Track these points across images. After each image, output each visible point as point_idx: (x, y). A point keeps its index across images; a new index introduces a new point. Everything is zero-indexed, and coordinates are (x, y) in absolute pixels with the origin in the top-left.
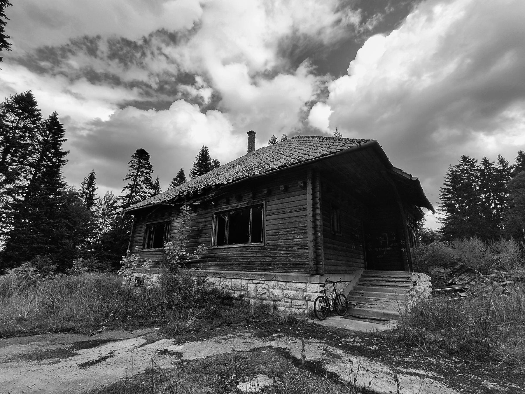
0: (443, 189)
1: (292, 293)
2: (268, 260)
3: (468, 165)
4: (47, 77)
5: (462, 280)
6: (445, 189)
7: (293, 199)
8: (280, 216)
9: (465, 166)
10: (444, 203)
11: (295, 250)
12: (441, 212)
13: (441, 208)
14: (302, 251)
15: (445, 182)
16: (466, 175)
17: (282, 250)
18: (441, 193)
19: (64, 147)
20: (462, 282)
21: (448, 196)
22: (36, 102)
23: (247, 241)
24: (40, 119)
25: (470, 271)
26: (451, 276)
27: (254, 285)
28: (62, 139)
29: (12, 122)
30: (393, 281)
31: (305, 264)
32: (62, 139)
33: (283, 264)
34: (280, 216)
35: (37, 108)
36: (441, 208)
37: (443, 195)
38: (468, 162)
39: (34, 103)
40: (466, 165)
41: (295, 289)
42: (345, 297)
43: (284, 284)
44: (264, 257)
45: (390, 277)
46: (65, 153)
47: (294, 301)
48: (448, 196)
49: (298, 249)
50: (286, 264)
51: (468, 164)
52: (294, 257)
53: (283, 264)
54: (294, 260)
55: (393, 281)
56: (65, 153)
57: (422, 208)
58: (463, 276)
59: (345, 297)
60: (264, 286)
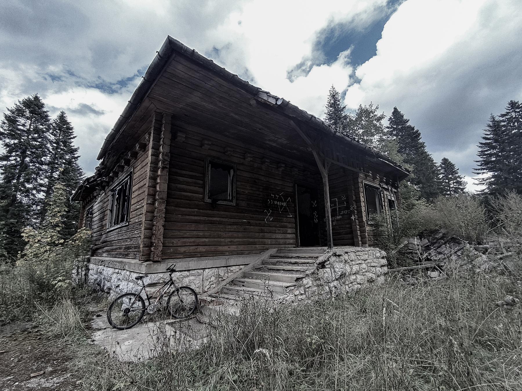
0: (481, 143)
3: (519, 112)
4: (116, 95)
5: (440, 253)
6: (484, 144)
9: (513, 114)
10: (484, 161)
12: (480, 171)
13: (480, 167)
15: (484, 136)
16: (516, 124)
18: (480, 150)
19: (75, 143)
20: (440, 256)
21: (489, 152)
22: (43, 104)
24: (48, 121)
25: (455, 241)
26: (427, 248)
28: (72, 136)
29: (24, 125)
30: (296, 263)
32: (72, 136)
35: (45, 109)
36: (480, 167)
37: (482, 151)
38: (518, 107)
39: (42, 106)
40: (516, 112)
42: (169, 299)
45: (298, 257)
46: (76, 150)
48: (489, 152)
51: (518, 110)
55: (296, 263)
56: (76, 150)
57: (327, 123)
58: (443, 249)
59: (169, 299)
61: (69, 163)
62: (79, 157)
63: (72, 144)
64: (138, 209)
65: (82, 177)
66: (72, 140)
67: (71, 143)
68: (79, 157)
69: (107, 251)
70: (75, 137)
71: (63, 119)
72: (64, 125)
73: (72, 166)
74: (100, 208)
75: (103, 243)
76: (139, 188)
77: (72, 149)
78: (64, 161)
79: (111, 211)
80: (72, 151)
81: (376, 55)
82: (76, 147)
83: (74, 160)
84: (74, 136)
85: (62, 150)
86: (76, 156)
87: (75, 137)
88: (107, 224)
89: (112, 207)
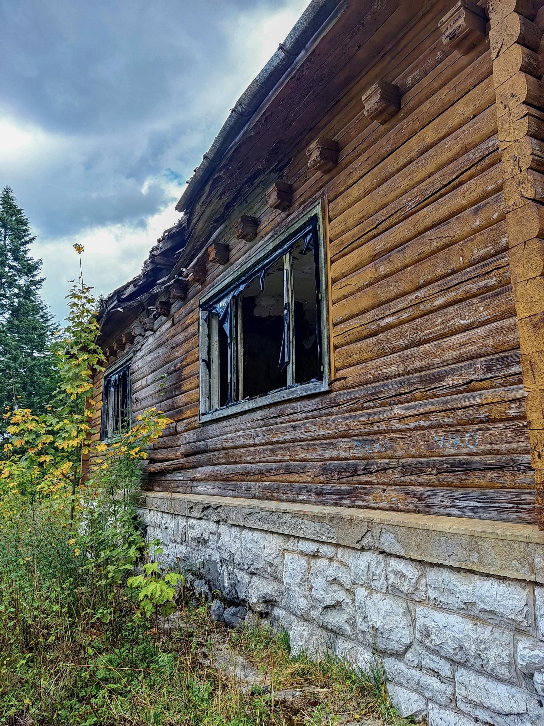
1: (453, 629)
2: (346, 450)
7: (429, 134)
8: (379, 244)
11: (456, 390)
14: (492, 395)
17: (399, 398)
23: (281, 383)
27: (304, 561)
28: (27, 238)
31: (515, 467)
32: (27, 238)
33: (404, 469)
34: (379, 244)
41: (468, 610)
43: (410, 570)
44: (329, 440)
47: (462, 674)
49: (469, 387)
50: (420, 469)
52: (454, 428)
53: (404, 469)
54: (452, 446)
56: (35, 267)
60: (333, 570)
61: (27, 294)
62: (43, 280)
63: (28, 255)
64: (389, 327)
65: (49, 323)
66: (28, 246)
67: (26, 252)
68: (43, 280)
69: (213, 478)
70: (33, 239)
71: (9, 203)
72: (12, 216)
73: (32, 301)
74: (159, 362)
75: (186, 456)
76: (374, 258)
77: (29, 264)
78: (17, 291)
79: (208, 364)
80: (30, 269)
81: (523, 69)
82: (36, 260)
83: (34, 287)
84: (31, 236)
85: (11, 267)
86: (37, 279)
87: (33, 239)
88: (202, 402)
89: (209, 354)
